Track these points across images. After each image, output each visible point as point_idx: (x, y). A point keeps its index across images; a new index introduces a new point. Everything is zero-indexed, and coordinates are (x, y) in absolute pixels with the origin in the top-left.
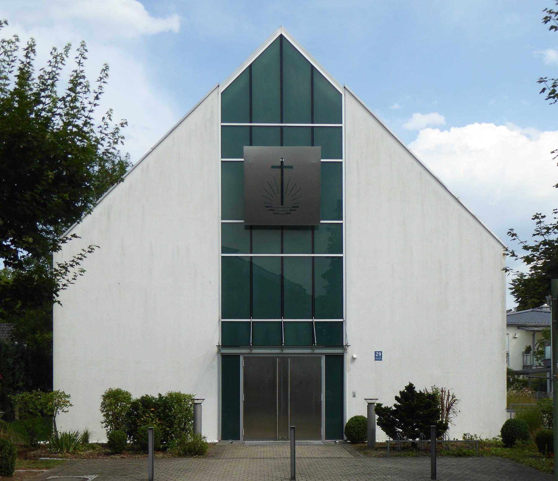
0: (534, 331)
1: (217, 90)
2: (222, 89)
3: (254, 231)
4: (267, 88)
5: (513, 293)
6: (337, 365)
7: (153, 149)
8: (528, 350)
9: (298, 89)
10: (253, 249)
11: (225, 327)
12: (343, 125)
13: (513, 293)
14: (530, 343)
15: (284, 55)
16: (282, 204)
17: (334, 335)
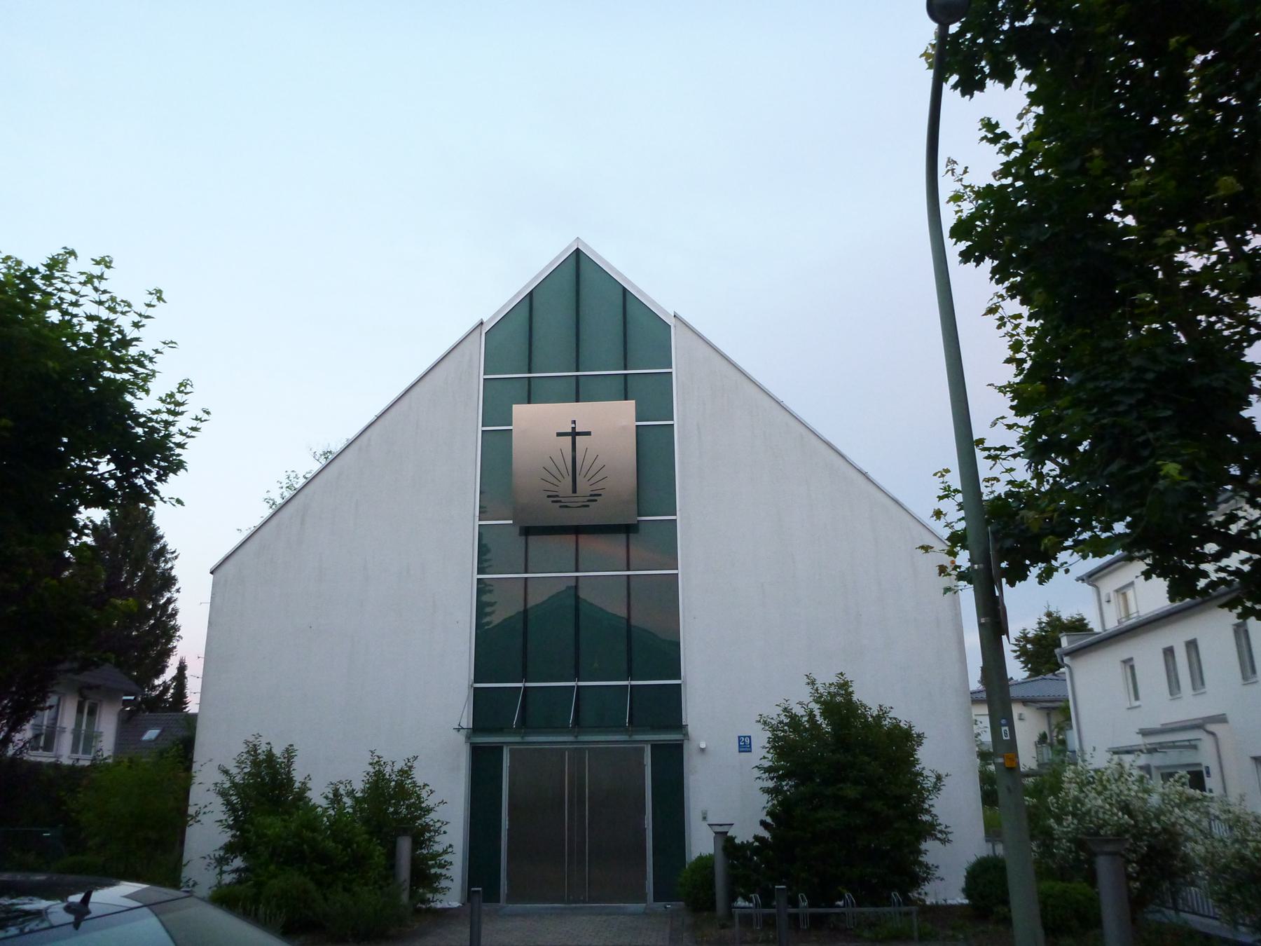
0: (1047, 708)
1: (478, 331)
2: (486, 328)
3: (532, 539)
4: (554, 327)
5: (1018, 657)
6: (671, 761)
7: (379, 417)
8: (1043, 739)
9: (601, 325)
10: (530, 564)
11: (480, 700)
12: (673, 370)
13: (1018, 657)
14: (1044, 728)
15: (582, 279)
16: (574, 491)
17: (665, 709)
